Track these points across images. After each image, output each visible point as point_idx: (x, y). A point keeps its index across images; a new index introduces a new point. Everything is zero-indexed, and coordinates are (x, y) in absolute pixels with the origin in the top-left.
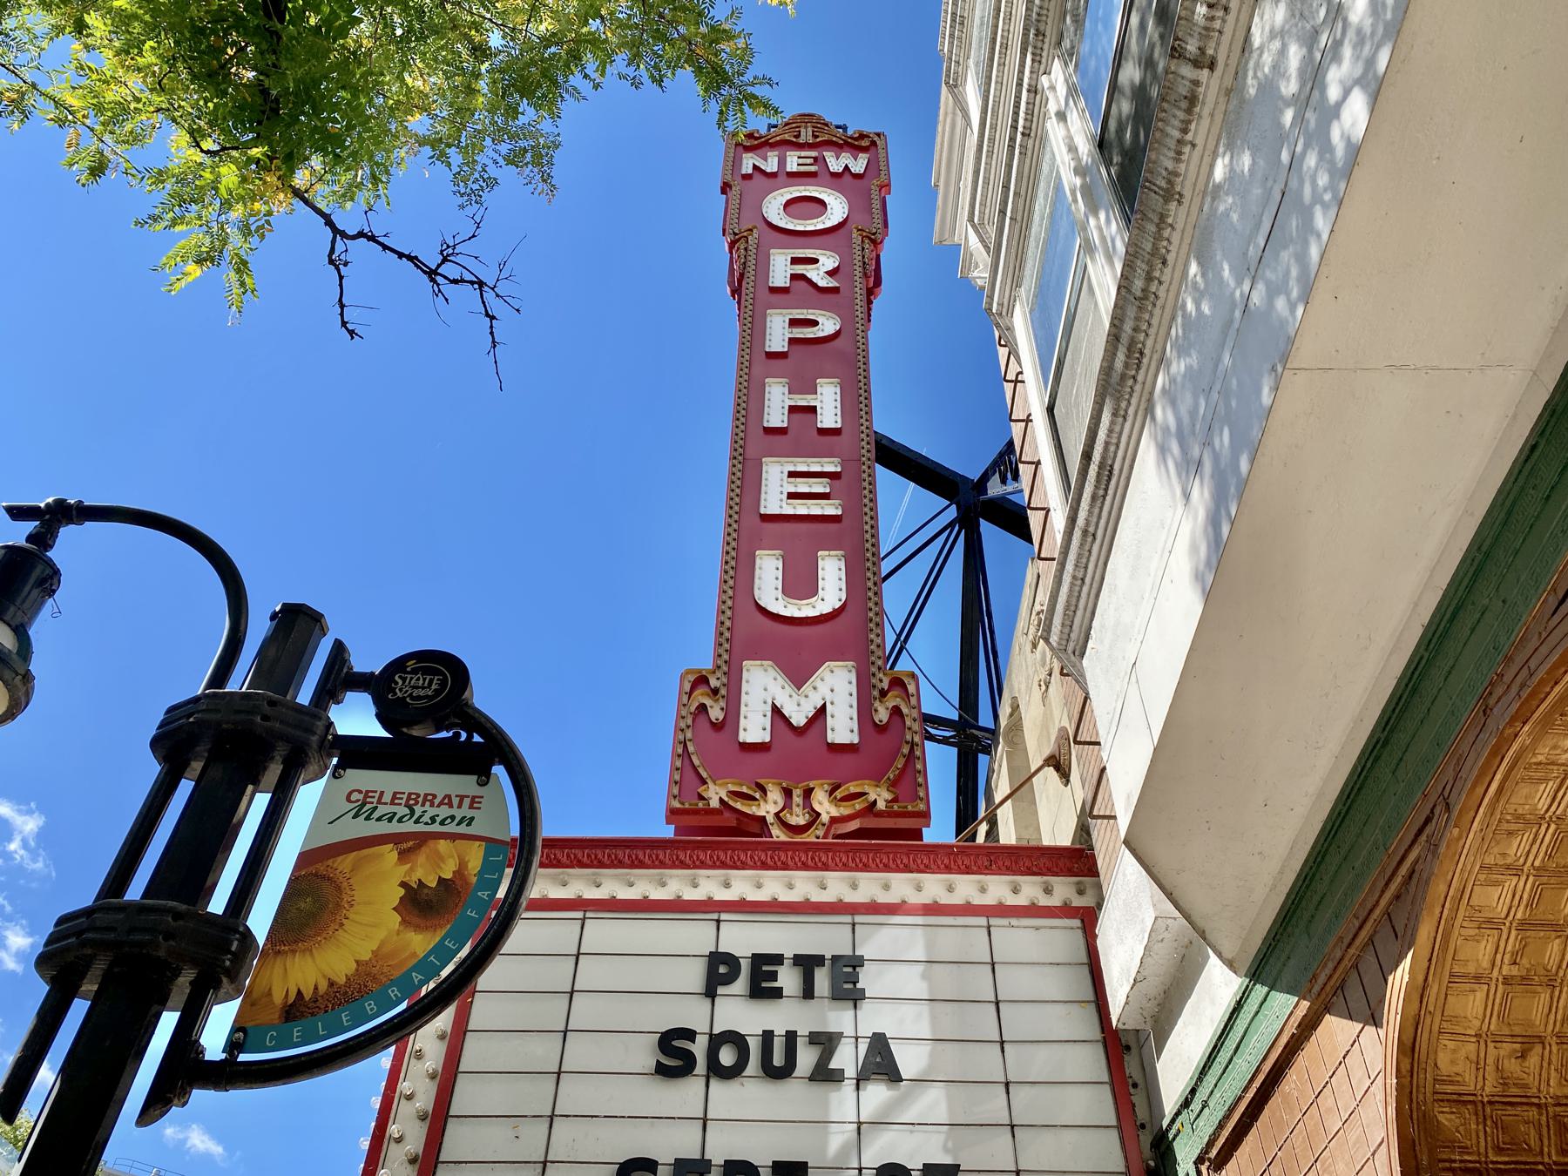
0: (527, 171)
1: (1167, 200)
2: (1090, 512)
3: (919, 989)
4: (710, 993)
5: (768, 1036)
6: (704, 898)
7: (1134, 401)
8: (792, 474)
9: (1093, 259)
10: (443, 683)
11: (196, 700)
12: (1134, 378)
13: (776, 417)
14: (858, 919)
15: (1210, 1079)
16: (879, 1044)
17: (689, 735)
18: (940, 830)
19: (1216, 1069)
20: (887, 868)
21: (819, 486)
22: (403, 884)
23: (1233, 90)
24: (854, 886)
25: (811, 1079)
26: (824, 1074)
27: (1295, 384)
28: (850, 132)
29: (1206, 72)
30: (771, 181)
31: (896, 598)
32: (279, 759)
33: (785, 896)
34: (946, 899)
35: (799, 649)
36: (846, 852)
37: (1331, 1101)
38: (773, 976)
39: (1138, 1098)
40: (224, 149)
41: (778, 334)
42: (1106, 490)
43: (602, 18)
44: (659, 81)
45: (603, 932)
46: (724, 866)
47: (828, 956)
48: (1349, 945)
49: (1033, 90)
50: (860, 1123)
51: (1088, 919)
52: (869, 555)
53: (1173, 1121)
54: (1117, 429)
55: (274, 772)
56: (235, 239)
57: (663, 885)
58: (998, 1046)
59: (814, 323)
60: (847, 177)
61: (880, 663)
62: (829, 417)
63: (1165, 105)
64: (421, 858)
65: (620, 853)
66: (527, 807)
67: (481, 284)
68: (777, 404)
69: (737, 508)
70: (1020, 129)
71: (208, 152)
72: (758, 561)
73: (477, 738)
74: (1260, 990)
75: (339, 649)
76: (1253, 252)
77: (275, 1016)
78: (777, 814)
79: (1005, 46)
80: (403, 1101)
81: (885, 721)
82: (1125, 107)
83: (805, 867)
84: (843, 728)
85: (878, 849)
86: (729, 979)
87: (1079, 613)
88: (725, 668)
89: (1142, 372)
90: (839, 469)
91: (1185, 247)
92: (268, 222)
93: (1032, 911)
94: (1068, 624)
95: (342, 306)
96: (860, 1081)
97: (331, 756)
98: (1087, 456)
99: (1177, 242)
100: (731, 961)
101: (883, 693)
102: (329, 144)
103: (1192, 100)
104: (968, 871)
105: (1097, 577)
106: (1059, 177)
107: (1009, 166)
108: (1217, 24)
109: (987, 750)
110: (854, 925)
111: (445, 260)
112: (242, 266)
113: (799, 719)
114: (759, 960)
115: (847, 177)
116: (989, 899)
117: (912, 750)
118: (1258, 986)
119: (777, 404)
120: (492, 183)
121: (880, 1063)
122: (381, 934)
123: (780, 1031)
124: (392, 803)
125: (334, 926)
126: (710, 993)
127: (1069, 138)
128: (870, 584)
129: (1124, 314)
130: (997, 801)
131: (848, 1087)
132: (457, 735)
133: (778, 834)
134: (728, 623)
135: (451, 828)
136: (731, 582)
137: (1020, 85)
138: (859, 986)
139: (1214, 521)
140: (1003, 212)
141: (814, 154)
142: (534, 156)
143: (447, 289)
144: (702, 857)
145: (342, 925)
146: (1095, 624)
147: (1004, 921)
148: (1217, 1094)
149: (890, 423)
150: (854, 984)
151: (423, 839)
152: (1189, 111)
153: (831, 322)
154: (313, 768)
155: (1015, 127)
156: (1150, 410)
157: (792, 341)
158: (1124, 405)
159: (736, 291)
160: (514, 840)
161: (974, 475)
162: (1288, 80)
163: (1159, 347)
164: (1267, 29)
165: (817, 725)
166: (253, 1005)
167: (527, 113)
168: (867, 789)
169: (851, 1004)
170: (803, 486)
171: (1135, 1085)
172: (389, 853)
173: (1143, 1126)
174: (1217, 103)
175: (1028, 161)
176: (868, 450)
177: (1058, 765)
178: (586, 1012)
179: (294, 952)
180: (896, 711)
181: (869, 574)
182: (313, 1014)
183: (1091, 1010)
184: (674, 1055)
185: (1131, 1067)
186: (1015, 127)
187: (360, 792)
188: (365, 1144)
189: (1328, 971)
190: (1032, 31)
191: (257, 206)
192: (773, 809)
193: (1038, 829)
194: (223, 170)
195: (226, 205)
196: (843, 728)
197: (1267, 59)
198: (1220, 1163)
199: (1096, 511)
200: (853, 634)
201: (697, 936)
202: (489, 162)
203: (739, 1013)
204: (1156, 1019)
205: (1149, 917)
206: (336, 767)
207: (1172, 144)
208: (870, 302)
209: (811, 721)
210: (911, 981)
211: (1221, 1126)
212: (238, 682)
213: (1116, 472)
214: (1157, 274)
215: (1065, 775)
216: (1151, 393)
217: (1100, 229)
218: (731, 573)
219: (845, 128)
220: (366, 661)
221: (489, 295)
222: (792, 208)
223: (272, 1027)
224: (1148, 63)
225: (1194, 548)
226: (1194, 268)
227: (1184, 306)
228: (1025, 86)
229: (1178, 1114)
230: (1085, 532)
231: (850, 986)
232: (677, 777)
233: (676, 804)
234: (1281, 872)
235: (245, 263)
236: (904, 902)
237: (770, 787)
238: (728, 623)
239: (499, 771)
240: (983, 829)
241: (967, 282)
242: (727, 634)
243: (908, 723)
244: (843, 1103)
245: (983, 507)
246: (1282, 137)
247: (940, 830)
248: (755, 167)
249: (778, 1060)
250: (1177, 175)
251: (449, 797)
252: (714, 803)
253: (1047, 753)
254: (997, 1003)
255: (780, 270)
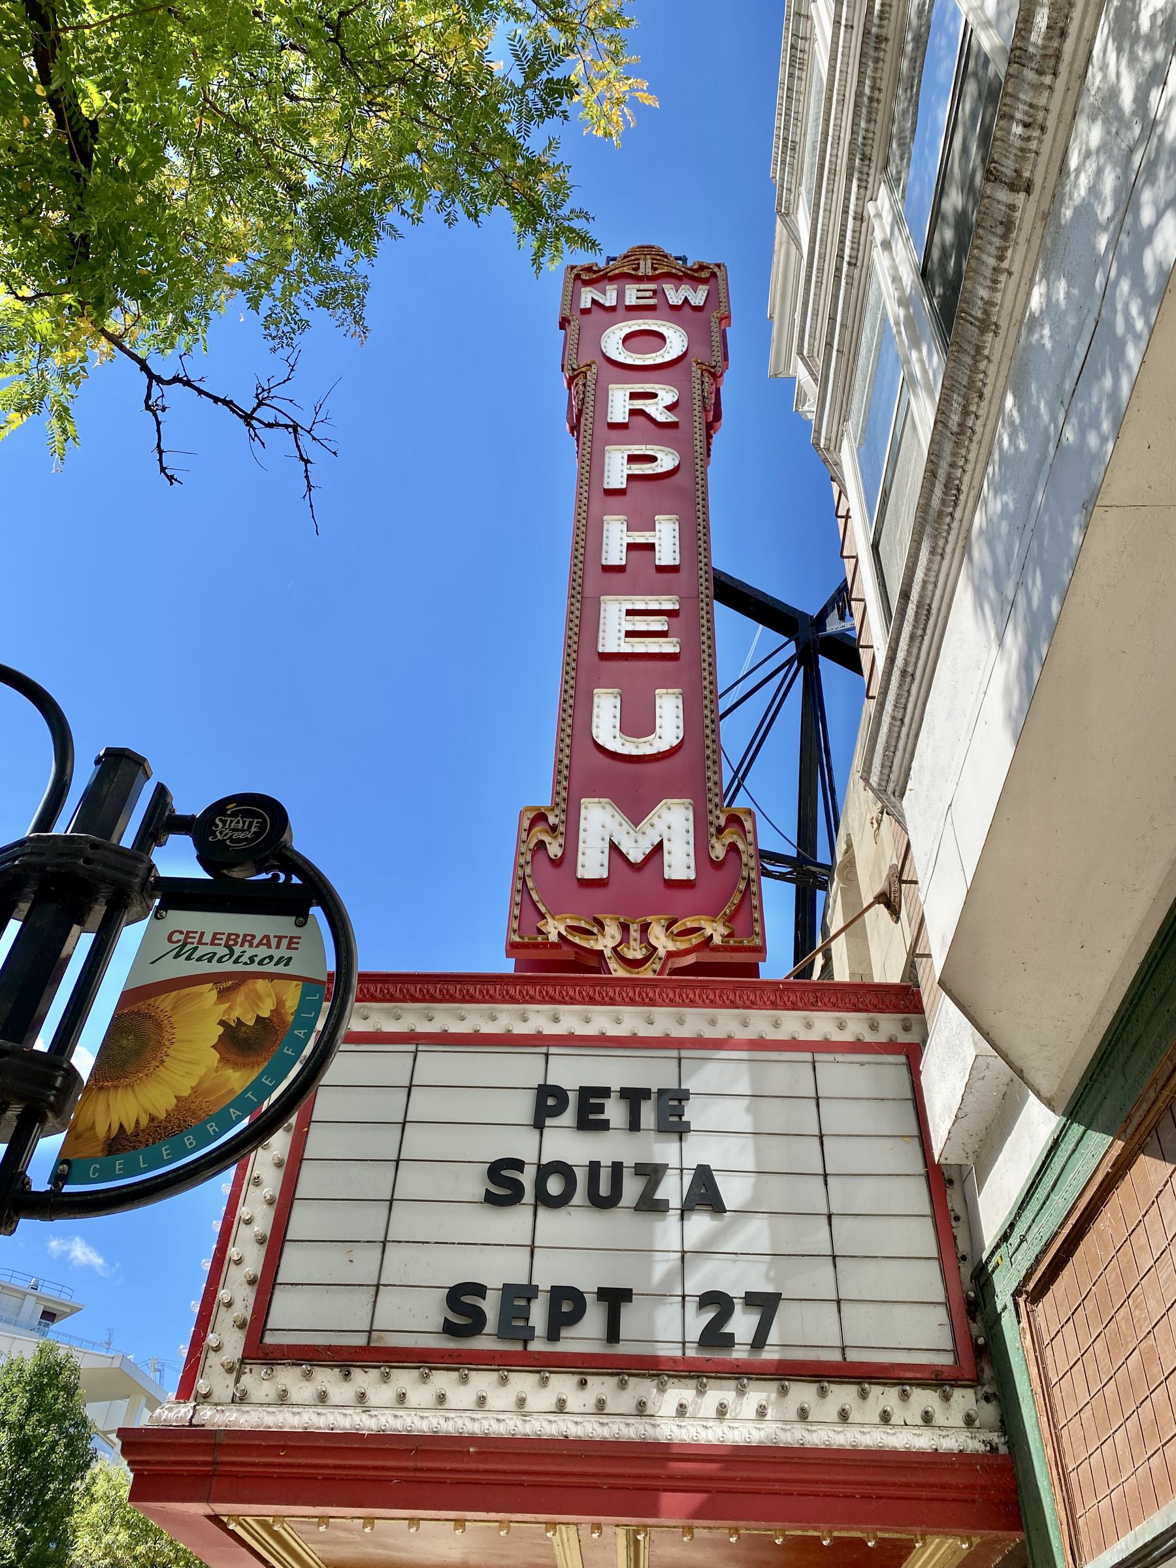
0: (339, 312)
1: (983, 331)
2: (909, 652)
3: (744, 1122)
4: (539, 1125)
5: (594, 1167)
6: (533, 1032)
7: (951, 539)
8: (630, 613)
9: (916, 395)
10: (262, 826)
11: (21, 843)
12: (951, 515)
13: (614, 554)
14: (684, 1053)
15: (1028, 1214)
16: (704, 1175)
17: (528, 871)
18: (777, 963)
19: (1034, 1205)
20: (713, 1004)
21: (657, 624)
22: (222, 1023)
23: (1049, 216)
24: (681, 1022)
25: (637, 1209)
26: (650, 1205)
27: (1107, 523)
28: (689, 264)
29: (1022, 195)
30: (611, 315)
31: (734, 735)
32: (102, 900)
33: (612, 1031)
34: (771, 1035)
35: (634, 784)
36: (674, 989)
37: (1143, 1240)
38: (600, 1109)
39: (960, 1231)
40: (38, 295)
41: (617, 471)
42: (924, 630)
43: (418, 152)
44: (474, 216)
45: (435, 1065)
46: (553, 1001)
47: (654, 1090)
48: (1164, 1087)
49: (860, 218)
50: (683, 1252)
51: (913, 1055)
52: (706, 692)
53: (992, 1254)
54: (935, 567)
55: (99, 911)
56: (55, 386)
57: (494, 1019)
58: (821, 1179)
59: (653, 459)
60: (687, 309)
61: (717, 800)
62: (667, 554)
63: (981, 231)
64: (240, 997)
65: (451, 989)
66: (343, 947)
67: (295, 427)
68: (616, 541)
69: (575, 647)
70: (846, 258)
71: (22, 299)
72: (596, 700)
73: (295, 880)
74: (1077, 1129)
75: (161, 792)
76: (1068, 385)
77: (96, 1149)
78: (614, 949)
79: (833, 172)
80: (242, 1225)
81: (721, 857)
82: (949, 235)
83: (632, 1002)
84: (680, 863)
85: (704, 986)
86: (558, 1111)
87: (899, 754)
88: (564, 806)
89: (959, 509)
90: (677, 607)
91: (1001, 380)
92: (83, 369)
93: (858, 1047)
94: (887, 764)
95: (161, 452)
96: (685, 1210)
97: (153, 897)
98: (905, 595)
99: (994, 373)
100: (559, 1093)
101: (720, 831)
102: (140, 289)
103: (1008, 225)
104: (794, 1007)
105: (916, 717)
106: (884, 308)
107: (835, 297)
108: (1033, 145)
109: (824, 886)
110: (680, 1059)
111: (259, 405)
112: (63, 414)
113: (636, 856)
114: (586, 1093)
115: (687, 309)
116: (814, 1036)
117: (748, 886)
118: (1075, 1125)
119: (616, 541)
120: (304, 325)
121: (704, 1194)
122: (199, 1071)
123: (606, 1161)
124: (212, 943)
125: (154, 1063)
126: (539, 1125)
127: (894, 268)
128: (707, 722)
129: (941, 449)
130: (833, 932)
131: (673, 1217)
132: (276, 877)
133: (618, 971)
134: (566, 761)
135: (270, 968)
136: (570, 721)
137: (846, 212)
138: (684, 1119)
139: (1026, 665)
140: (829, 345)
141: (653, 286)
142: (345, 297)
143: (262, 432)
144: (531, 992)
145: (162, 1062)
146: (914, 764)
147: (830, 1057)
148: (1035, 1229)
149: (726, 559)
150: (680, 1116)
151: (242, 978)
152: (1005, 237)
153: (670, 457)
154: (136, 909)
155: (840, 257)
156: (967, 549)
157: (631, 478)
158: (941, 542)
159: (575, 428)
160: (330, 975)
161: (813, 611)
162: (1104, 204)
163: (976, 483)
164: (1083, 151)
165: (656, 859)
166: (78, 1138)
167: (344, 254)
168: (703, 924)
169: (676, 1136)
170: (641, 624)
171: (957, 1218)
172: (209, 993)
173: (964, 1258)
174: (1033, 228)
175: (854, 291)
176: (706, 588)
177: (889, 901)
178: (417, 1142)
179: (116, 1087)
180: (733, 848)
181: (707, 712)
182: (134, 1148)
183: (915, 1144)
184: (503, 1184)
185: (954, 1200)
186: (840, 257)
187: (181, 933)
188: (207, 1265)
189: (1141, 1112)
190: (858, 156)
191: (71, 353)
192: (611, 943)
193: (870, 965)
194: (37, 317)
195: (45, 351)
196: (680, 863)
197: (1084, 181)
198: (1036, 1296)
199: (915, 651)
200: (689, 770)
201: (527, 1070)
202: (300, 304)
203: (566, 1144)
204: (977, 1155)
205: (970, 1054)
206: (158, 908)
207: (988, 273)
208: (709, 437)
209: (648, 858)
210: (736, 1114)
211: (1038, 1260)
212: (62, 827)
213: (934, 611)
214: (973, 408)
215: (895, 912)
216: (969, 531)
217: (921, 361)
218: (570, 711)
219: (684, 259)
220: (189, 802)
221: (305, 439)
222: (627, 343)
223: (94, 1159)
224: (969, 188)
225: (1007, 693)
226: (1010, 401)
227: (1001, 442)
228: (851, 214)
229: (997, 1247)
230: (904, 672)
231: (676, 1119)
232: (517, 912)
233: (516, 939)
234: (1099, 1013)
235: (66, 410)
236: (730, 1037)
237: (607, 922)
238: (566, 761)
239: (316, 912)
240: (819, 961)
241: (799, 418)
242: (566, 772)
243: (745, 859)
244: (668, 1232)
245: (817, 642)
246: (1098, 262)
247: (777, 963)
248: (594, 301)
249: (604, 1189)
250: (993, 304)
251: (267, 937)
252: (553, 938)
253: (877, 890)
254: (821, 1137)
255: (619, 406)
